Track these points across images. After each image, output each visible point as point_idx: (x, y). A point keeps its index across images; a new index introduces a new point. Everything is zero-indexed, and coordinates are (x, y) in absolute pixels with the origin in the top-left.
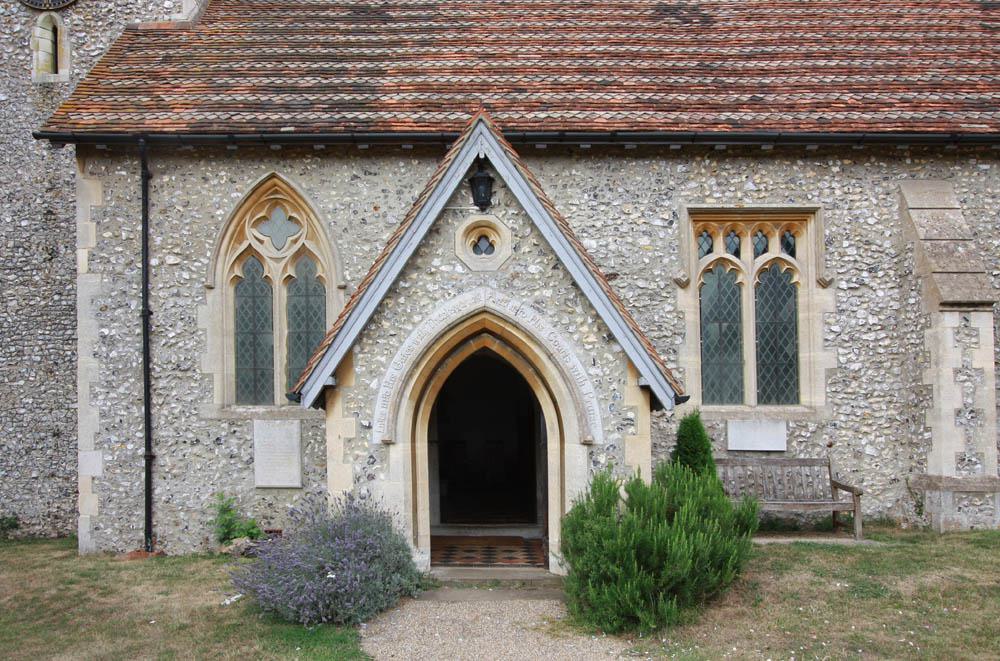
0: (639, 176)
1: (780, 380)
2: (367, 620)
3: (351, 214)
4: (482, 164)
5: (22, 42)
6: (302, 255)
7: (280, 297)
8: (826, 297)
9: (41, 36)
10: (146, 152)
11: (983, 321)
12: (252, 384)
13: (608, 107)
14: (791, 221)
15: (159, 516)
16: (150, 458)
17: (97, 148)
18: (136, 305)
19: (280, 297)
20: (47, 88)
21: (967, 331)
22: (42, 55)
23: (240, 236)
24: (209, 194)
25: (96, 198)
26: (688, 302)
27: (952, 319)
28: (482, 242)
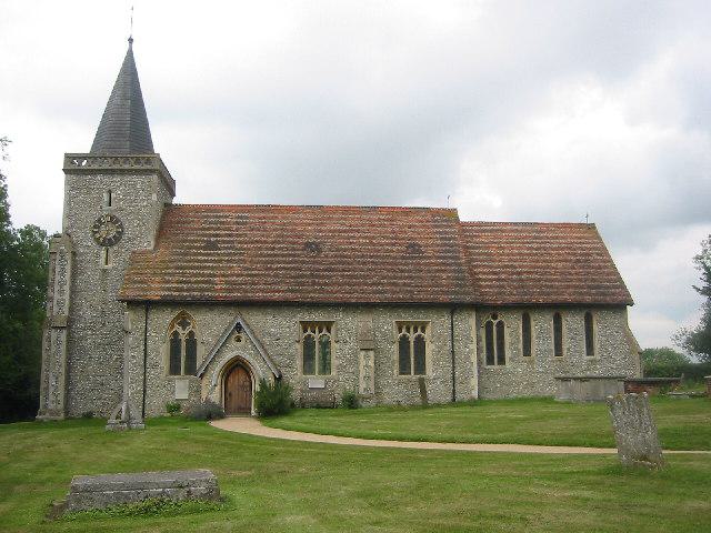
0: (286, 312)
1: (326, 368)
2: (43, 235)
3: (208, 327)
4: (238, 324)
5: (98, 256)
6: (191, 334)
7: (184, 344)
8: (337, 346)
9: (103, 253)
10: (147, 305)
11: (372, 354)
12: (174, 370)
13: (279, 291)
14: (328, 325)
15: (147, 408)
16: (145, 391)
17: (133, 304)
18: (142, 347)
19: (184, 344)
20: (105, 271)
21: (366, 357)
22: (103, 260)
23: (173, 326)
24: (163, 320)
25: (131, 319)
26: (299, 347)
27: (363, 353)
28: (239, 340)
